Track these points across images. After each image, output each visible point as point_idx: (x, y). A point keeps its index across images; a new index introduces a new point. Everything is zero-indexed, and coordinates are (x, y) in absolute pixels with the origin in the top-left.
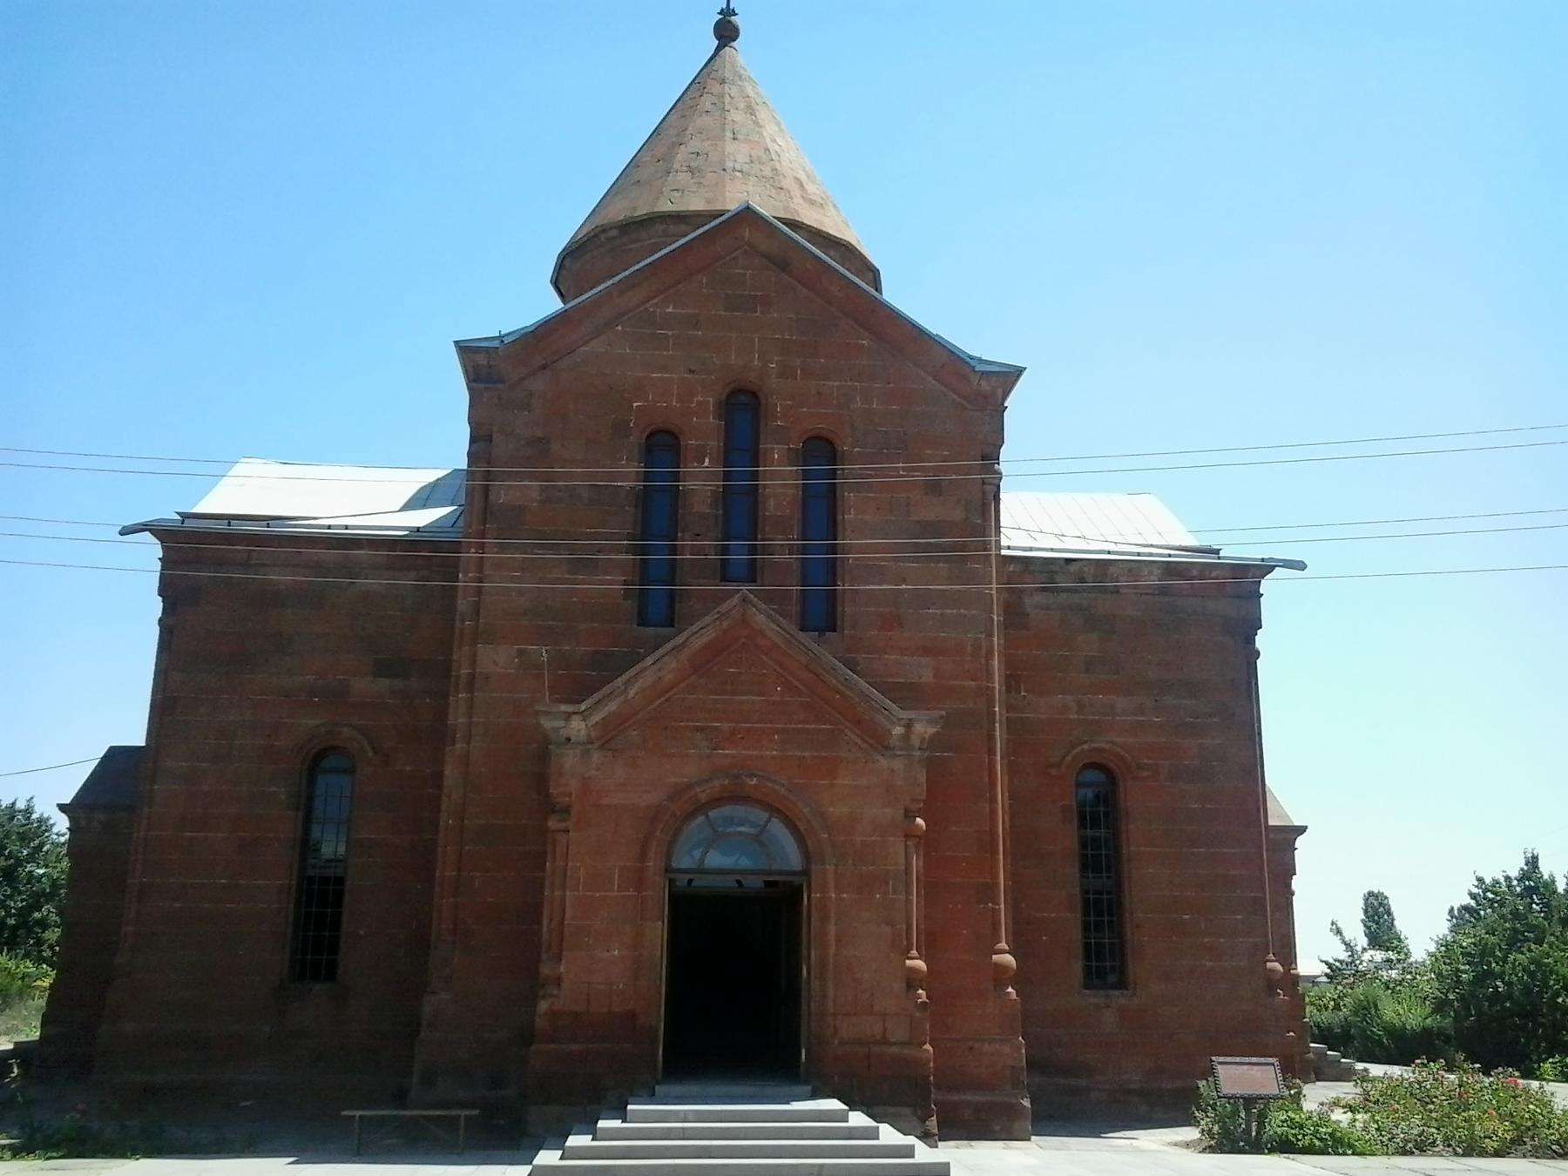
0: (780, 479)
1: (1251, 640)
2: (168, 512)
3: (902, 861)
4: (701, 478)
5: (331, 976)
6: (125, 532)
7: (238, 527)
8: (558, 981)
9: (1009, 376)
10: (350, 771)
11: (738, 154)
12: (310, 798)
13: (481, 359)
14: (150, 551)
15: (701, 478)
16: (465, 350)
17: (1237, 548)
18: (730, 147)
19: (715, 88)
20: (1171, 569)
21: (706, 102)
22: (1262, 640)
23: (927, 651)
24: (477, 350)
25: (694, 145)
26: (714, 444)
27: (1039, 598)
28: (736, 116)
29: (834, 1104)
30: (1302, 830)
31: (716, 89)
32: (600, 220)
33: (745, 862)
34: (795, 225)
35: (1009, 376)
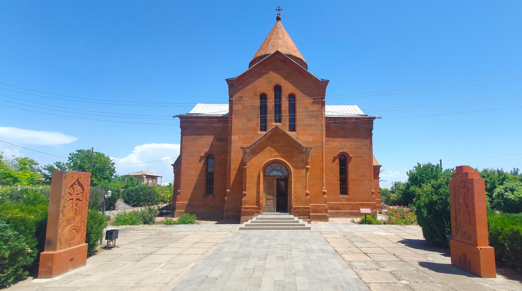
0: (285, 104)
1: (371, 131)
2: (184, 113)
3: (255, 190)
4: (271, 104)
5: (212, 193)
6: (174, 117)
7: (199, 115)
8: (245, 195)
9: (326, 82)
10: (214, 158)
11: (281, 42)
12: (208, 164)
13: (230, 82)
14: (178, 120)
15: (271, 104)
16: (227, 80)
17: (370, 115)
18: (279, 41)
19: (277, 30)
20: (357, 119)
21: (275, 33)
22: (373, 132)
23: (311, 135)
24: (229, 81)
25: (273, 41)
26: (273, 96)
27: (333, 125)
28: (280, 35)
29: (292, 216)
30: (381, 166)
31: (277, 30)
32: (256, 56)
33: (281, 174)
34: (290, 56)
35: (326, 82)
